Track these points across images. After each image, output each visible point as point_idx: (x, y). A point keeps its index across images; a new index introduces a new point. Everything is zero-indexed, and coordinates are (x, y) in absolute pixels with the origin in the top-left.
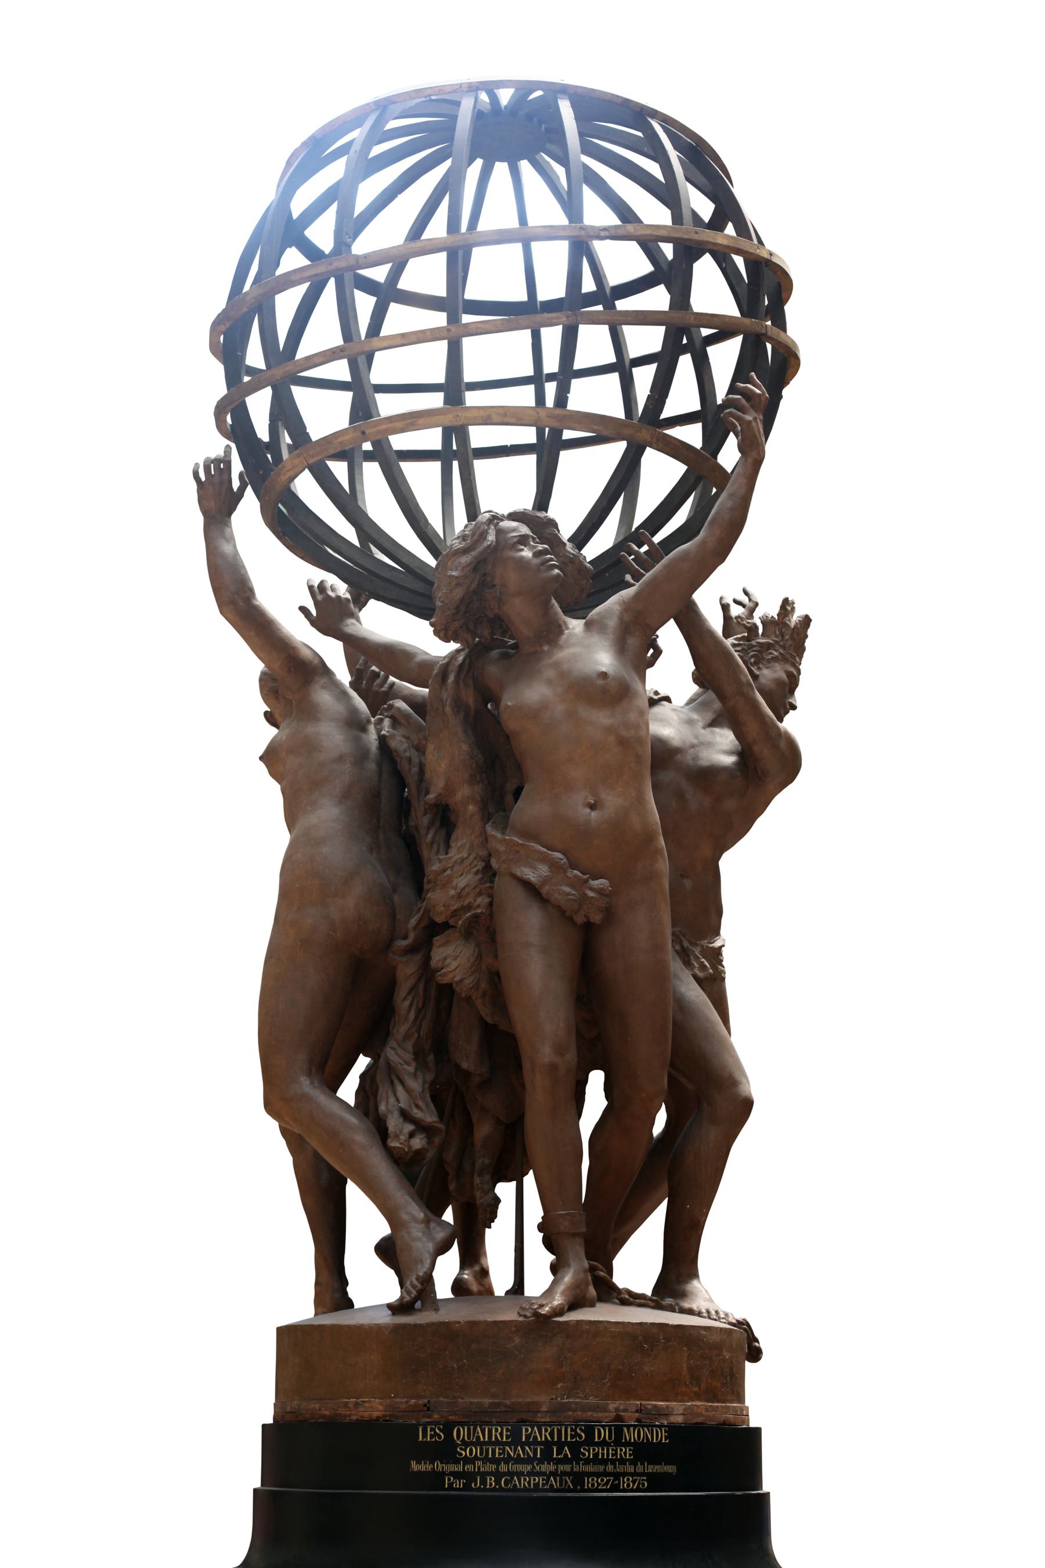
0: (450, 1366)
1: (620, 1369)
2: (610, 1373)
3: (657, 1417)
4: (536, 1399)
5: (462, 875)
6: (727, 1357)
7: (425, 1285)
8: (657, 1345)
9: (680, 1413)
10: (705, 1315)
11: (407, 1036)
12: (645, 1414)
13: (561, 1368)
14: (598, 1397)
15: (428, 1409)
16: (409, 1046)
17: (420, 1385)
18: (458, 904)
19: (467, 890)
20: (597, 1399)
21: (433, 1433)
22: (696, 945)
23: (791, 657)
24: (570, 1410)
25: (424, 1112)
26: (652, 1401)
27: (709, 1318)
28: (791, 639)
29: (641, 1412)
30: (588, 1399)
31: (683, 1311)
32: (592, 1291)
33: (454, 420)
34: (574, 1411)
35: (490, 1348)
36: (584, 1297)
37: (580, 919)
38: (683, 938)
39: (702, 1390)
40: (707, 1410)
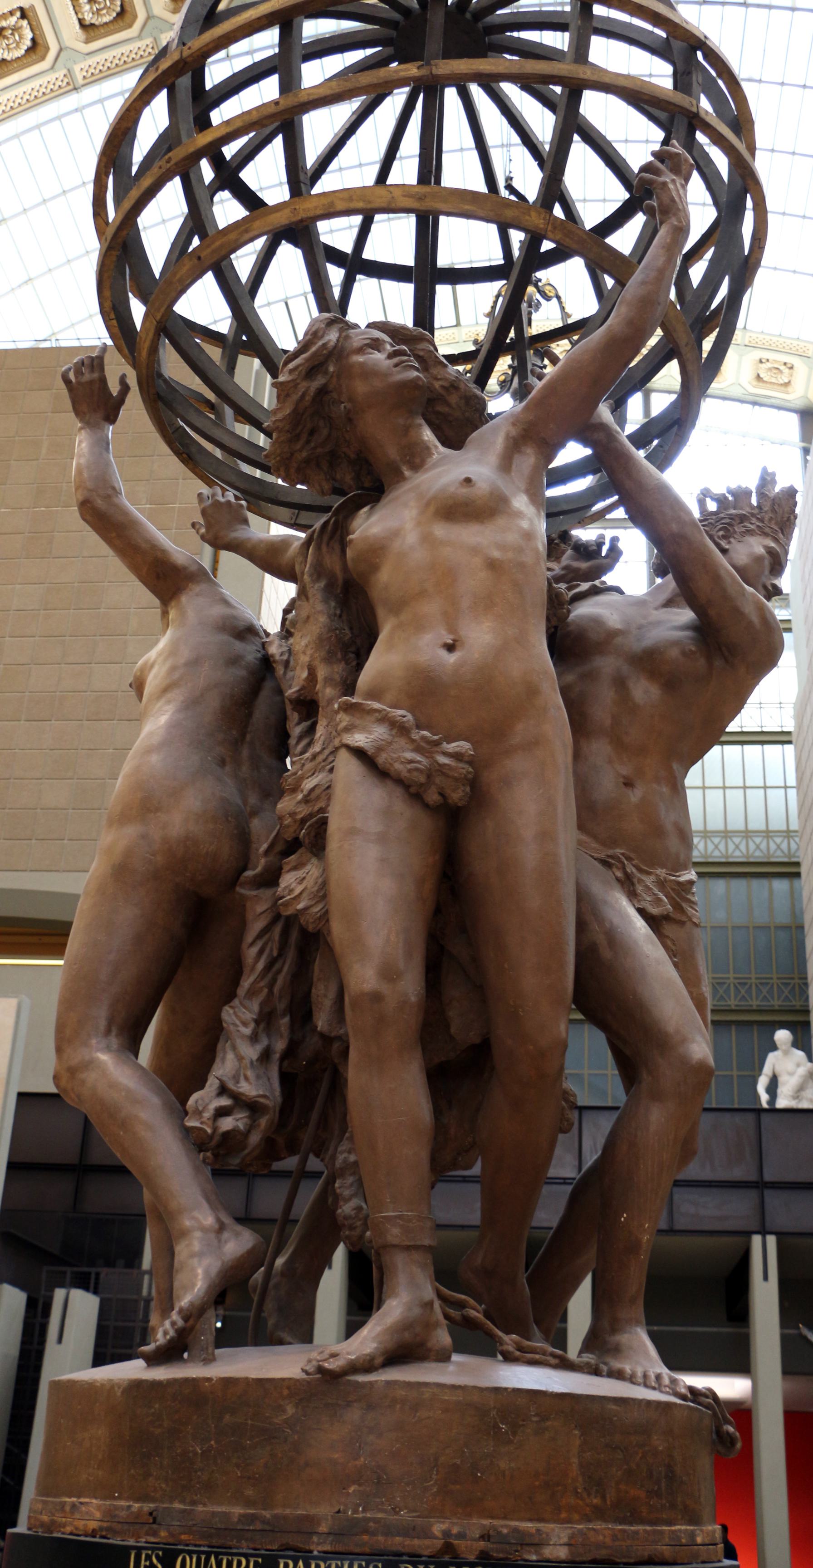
0: (191, 1449)
1: (455, 1464)
2: (437, 1471)
3: (519, 1549)
4: (313, 1511)
5: (313, 774)
6: (661, 1448)
7: (191, 1322)
8: (523, 1425)
9: (562, 1542)
10: (640, 1380)
11: (251, 993)
12: (496, 1543)
13: (356, 1459)
14: (415, 1511)
15: (154, 1522)
16: (255, 1006)
17: (151, 1479)
18: (305, 811)
19: (317, 792)
20: (414, 1514)
21: (148, 1563)
22: (649, 873)
23: (772, 532)
24: (366, 1531)
25: (250, 1083)
26: (512, 1519)
27: (646, 1386)
28: (772, 511)
29: (489, 1541)
30: (397, 1513)
31: (618, 1375)
32: (443, 1337)
33: (292, 215)
34: (373, 1534)
35: (249, 1422)
36: (422, 1344)
37: (432, 797)
38: (626, 862)
39: (608, 1503)
40: (614, 1537)
